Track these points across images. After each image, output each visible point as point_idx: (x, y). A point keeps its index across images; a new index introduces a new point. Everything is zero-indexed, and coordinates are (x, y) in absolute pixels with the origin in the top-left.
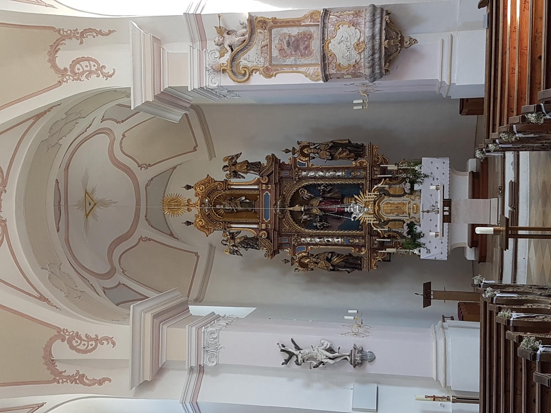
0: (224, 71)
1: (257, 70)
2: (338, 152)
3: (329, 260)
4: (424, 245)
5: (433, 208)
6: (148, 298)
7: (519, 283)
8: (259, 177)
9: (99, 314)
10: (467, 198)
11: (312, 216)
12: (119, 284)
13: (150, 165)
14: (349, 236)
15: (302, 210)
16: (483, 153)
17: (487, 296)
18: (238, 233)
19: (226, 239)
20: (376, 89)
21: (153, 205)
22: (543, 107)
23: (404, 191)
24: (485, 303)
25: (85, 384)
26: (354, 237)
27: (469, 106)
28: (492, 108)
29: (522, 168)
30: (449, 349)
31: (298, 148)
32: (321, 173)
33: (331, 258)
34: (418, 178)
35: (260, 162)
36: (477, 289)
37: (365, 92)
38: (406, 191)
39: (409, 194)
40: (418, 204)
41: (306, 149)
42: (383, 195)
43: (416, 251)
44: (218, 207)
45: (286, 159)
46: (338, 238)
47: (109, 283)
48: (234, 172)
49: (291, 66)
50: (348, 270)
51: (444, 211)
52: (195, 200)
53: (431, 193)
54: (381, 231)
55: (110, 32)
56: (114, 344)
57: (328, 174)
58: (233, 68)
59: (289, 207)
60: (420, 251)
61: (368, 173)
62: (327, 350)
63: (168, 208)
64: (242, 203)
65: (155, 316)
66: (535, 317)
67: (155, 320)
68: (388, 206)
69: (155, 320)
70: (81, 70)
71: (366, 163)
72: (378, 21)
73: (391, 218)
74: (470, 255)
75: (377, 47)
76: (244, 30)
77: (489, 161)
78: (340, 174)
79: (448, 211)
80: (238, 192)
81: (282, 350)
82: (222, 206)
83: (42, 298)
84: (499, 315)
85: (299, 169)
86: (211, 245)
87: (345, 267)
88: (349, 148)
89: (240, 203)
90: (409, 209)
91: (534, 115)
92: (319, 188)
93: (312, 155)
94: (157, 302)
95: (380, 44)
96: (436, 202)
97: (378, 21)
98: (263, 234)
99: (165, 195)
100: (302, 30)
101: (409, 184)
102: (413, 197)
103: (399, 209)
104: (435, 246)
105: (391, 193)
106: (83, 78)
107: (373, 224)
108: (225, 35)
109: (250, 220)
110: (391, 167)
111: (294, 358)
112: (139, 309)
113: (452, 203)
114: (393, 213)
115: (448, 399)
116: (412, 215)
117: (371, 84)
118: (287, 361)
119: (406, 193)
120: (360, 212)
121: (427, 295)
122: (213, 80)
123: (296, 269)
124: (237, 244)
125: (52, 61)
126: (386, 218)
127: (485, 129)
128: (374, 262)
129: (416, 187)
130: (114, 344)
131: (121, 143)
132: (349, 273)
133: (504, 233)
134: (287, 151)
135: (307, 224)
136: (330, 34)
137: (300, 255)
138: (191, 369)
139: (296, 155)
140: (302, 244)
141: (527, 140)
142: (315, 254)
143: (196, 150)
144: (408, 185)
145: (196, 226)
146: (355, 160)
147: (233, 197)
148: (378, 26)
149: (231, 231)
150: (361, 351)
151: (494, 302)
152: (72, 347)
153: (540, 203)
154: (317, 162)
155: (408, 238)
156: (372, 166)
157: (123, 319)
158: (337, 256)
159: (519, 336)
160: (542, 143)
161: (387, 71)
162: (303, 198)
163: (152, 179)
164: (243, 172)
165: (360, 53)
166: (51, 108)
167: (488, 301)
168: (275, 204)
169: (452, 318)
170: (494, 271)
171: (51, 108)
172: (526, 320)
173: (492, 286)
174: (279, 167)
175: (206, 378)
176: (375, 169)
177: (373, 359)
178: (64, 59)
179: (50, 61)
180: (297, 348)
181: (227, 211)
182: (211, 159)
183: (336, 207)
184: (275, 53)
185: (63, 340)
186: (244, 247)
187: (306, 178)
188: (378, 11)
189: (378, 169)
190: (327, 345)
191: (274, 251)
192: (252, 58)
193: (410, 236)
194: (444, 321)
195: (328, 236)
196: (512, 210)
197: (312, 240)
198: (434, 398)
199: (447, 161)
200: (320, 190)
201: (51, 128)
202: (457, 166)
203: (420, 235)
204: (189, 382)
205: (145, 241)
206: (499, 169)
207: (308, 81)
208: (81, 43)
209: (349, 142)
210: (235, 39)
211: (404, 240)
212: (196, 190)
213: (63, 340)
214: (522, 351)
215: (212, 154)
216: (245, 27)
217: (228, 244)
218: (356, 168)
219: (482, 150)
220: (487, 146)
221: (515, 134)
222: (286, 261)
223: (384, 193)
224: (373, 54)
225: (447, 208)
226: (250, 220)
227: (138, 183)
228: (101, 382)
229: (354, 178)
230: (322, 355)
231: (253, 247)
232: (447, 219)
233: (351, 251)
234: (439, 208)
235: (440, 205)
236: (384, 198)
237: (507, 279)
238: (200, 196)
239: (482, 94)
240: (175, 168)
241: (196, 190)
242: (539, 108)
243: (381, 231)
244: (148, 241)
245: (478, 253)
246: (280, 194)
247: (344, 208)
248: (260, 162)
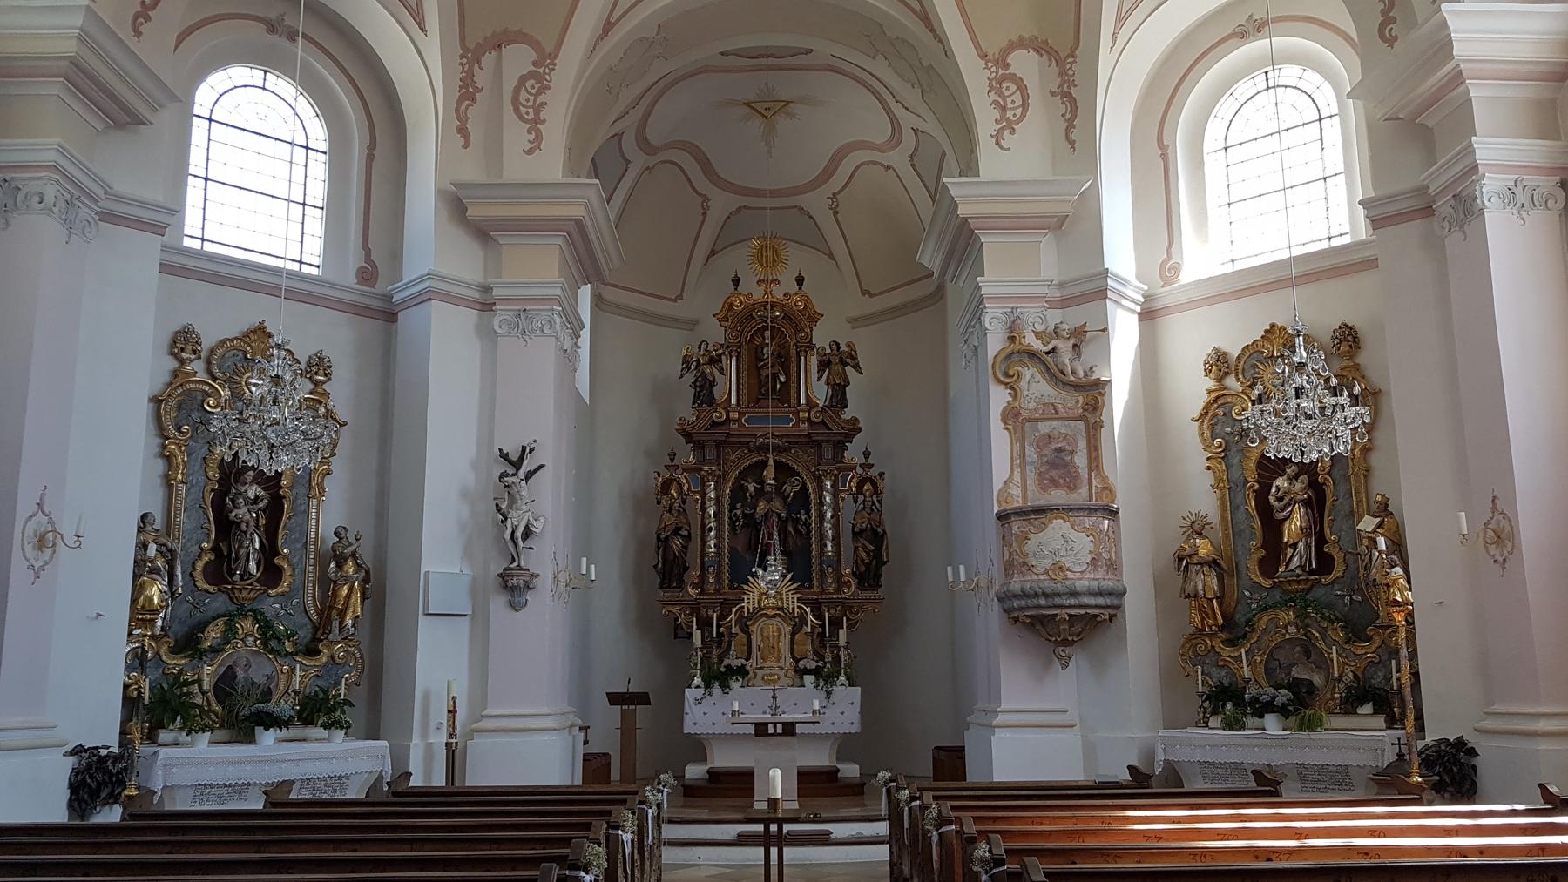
0: (1012, 339)
1: (1015, 397)
3: (676, 531)
7: (663, 849)
9: (579, 130)
12: (628, 162)
16: (886, 783)
18: (721, 371)
19: (710, 348)
21: (769, 222)
25: (459, 103)
30: (538, 737)
31: (873, 472)
32: (829, 515)
43: (697, 681)
44: (768, 333)
45: (853, 452)
47: (629, 144)
49: (1023, 455)
51: (775, 724)
52: (778, 293)
53: (803, 703)
55: (1072, 143)
56: (530, 152)
57: (828, 526)
58: (1017, 355)
62: (527, 527)
64: (775, 376)
65: (579, 223)
68: (774, 632)
70: (1007, 93)
71: (847, 592)
72: (1100, 601)
73: (753, 637)
75: (1058, 601)
76: (1082, 374)
80: (793, 369)
81: (524, 448)
82: (768, 340)
83: (608, 27)
86: (696, 323)
87: (664, 559)
90: (771, 668)
93: (861, 498)
95: (1062, 607)
97: (1100, 601)
98: (719, 416)
100: (1084, 473)
102: (791, 673)
103: (770, 650)
104: (705, 712)
106: (994, 96)
108: (1072, 341)
110: (843, 634)
111: (511, 470)
112: (592, 194)
115: (451, 736)
116: (760, 673)
117: (992, 593)
118: (505, 456)
119: (797, 661)
125: (1021, 43)
129: (809, 679)
130: (530, 152)
131: (875, 163)
134: (867, 454)
135: (738, 492)
136: (1077, 521)
138: (486, 289)
139: (860, 470)
140: (703, 484)
144: (813, 665)
145: (732, 295)
146: (854, 574)
147: (785, 362)
148: (1092, 601)
150: (528, 587)
152: (523, 80)
154: (848, 508)
156: (843, 602)
157: (571, 168)
161: (1016, 620)
165: (1046, 572)
166: (940, 41)
169: (586, 742)
171: (940, 41)
175: (472, 315)
177: (515, 606)
178: (1025, 64)
179: (1021, 39)
180: (529, 475)
182: (849, 321)
184: (1044, 428)
185: (535, 63)
188: (1116, 602)
190: (537, 527)
192: (1036, 386)
195: (718, 529)
197: (712, 500)
198: (452, 712)
199: (855, 729)
201: (904, 41)
202: (846, 746)
203: (725, 687)
204: (465, 284)
206: (843, 813)
207: (997, 485)
208: (1053, 94)
210: (1066, 357)
213: (535, 63)
214: (581, 847)
215: (857, 322)
216: (1086, 375)
218: (838, 575)
222: (672, 456)
223: (798, 624)
224: (1046, 595)
225: (780, 730)
228: (462, 130)
229: (822, 573)
230: (518, 519)
231: (696, 397)
232: (761, 729)
234: (770, 716)
235: (786, 717)
237: (669, 831)
242: (999, 862)
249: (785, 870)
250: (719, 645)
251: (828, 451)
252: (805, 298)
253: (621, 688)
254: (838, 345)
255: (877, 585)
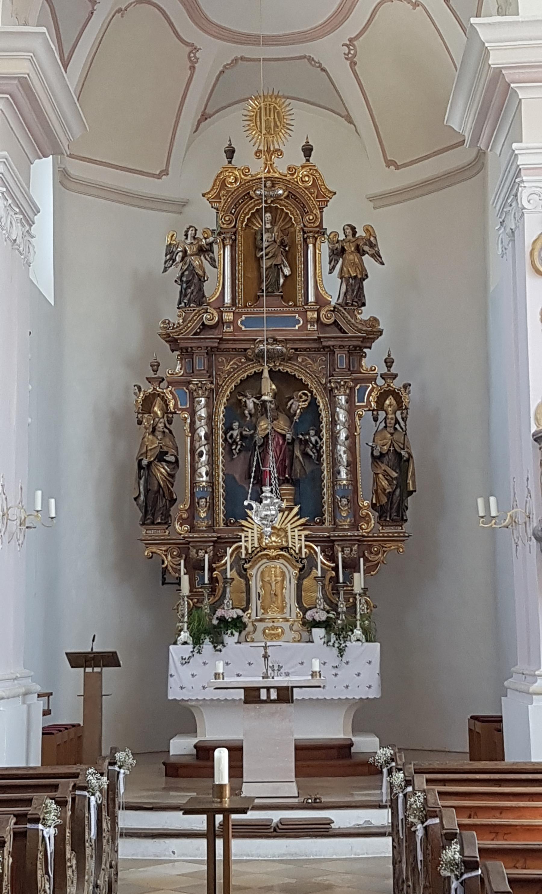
2: (388, 470)
3: (161, 457)
4: (199, 652)
5: (276, 668)
6: (66, 67)
8: (333, 303)
10: (297, 736)
11: (254, 419)
13: (353, 64)
14: (213, 498)
15: (264, 398)
16: (387, 762)
17: (90, 777)
19: (199, 235)
20: (520, 543)
21: (265, 79)
22: (474, 874)
23: (310, 609)
24: (76, 776)
26: (212, 508)
27: (487, 733)
28: (478, 776)
29: (359, 841)
31: (396, 384)
32: (343, 435)
33: (165, 461)
34: (338, 635)
35: (364, 305)
36: (104, 758)
37: (514, 521)
38: (309, 613)
39: (304, 618)
40: (284, 638)
41: (394, 402)
42: (301, 566)
43: (184, 636)
45: (373, 360)
46: (207, 474)
48: (343, 250)
50: (142, 498)
51: (268, 689)
52: (281, 167)
53: (305, 662)
54: (226, 563)
57: (341, 449)
59: (270, 372)
60: (185, 643)
61: (345, 533)
63: (260, 108)
64: (278, 268)
65: (24, 83)
66: (47, 873)
67: (16, 82)
68: (279, 576)
69: (16, 82)
71: (365, 529)
73: (252, 583)
74: (181, 746)
77: (372, 778)
78: (343, 475)
79: (268, 697)
82: (269, 225)
84: (49, 801)
85: (351, 389)
86: (184, 204)
87: (147, 491)
88: (398, 492)
89: (275, 265)
90: (273, 620)
91: (457, 856)
92: (312, 432)
94: (57, 89)
96: (287, 674)
98: (210, 317)
99: (288, 101)
101: (324, 618)
102: (298, 626)
103: (272, 598)
104: (195, 673)
105: (305, 582)
107: (240, 547)
109: (240, 289)
110: (359, 581)
112: (38, 45)
113: (285, 705)
114: (263, 587)
116: (260, 626)
117: (530, 531)
120: (262, 519)
121: (93, 659)
122: (537, 197)
123: (140, 389)
124: (188, 259)
126: (253, 572)
127: (436, 765)
128: (160, 550)
129: (318, 633)
132: (136, 499)
133: (218, 806)
134: (389, 363)
135: (235, 408)
137: (170, 397)
139: (380, 381)
141: (412, 850)
142: (171, 427)
143: (388, 166)
144: (322, 616)
146: (373, 506)
147: (288, 249)
149: (215, 246)
151: (78, 792)
153: (288, 880)
154: (367, 427)
155: (211, 620)
158: (169, 474)
159: (4, 842)
160: (407, 879)
162: (290, 398)
163: (323, 70)
164: (342, 269)
167: (79, 781)
168: (275, 340)
169: (47, 713)
170: (145, 794)
172: (40, 856)
173: (112, 789)
174: (355, 347)
176: (355, 548)
181: (259, 238)
182: (371, 199)
183: (271, 466)
186: (183, 274)
187: (333, 404)
189: (354, 554)
191: (176, 340)
193: (215, 622)
194: (39, 696)
195: (212, 454)
196: (273, 825)
197: (200, 422)
199: (374, 694)
200: (308, 434)
202: (363, 715)
203: (218, 642)
205: (189, 57)
206: (359, 797)
209: (411, 493)
211: (208, 611)
212: (303, 167)
215: (379, 200)
217: (189, 241)
218: (355, 507)
219: (393, 760)
220: (400, 770)
221: (423, 823)
222: (155, 367)
225: (274, 695)
226: (240, 289)
227: (313, 40)
231: (183, 295)
232: (252, 695)
233: (182, 502)
234: (277, 679)
235: (281, 680)
236: (295, 567)
237: (127, 820)
238: (289, 177)
239: (512, 756)
240: (349, 120)
241: (303, 167)
242: (471, 865)
243: (226, 563)
244: (189, 64)
245: (184, 760)
246: (299, 349)
247: (271, 485)
248: (364, 305)
249: (233, 867)
250: (213, 591)
251: (341, 359)
252: (313, 169)
253: (84, 647)
254: (353, 229)
255: (401, 519)
